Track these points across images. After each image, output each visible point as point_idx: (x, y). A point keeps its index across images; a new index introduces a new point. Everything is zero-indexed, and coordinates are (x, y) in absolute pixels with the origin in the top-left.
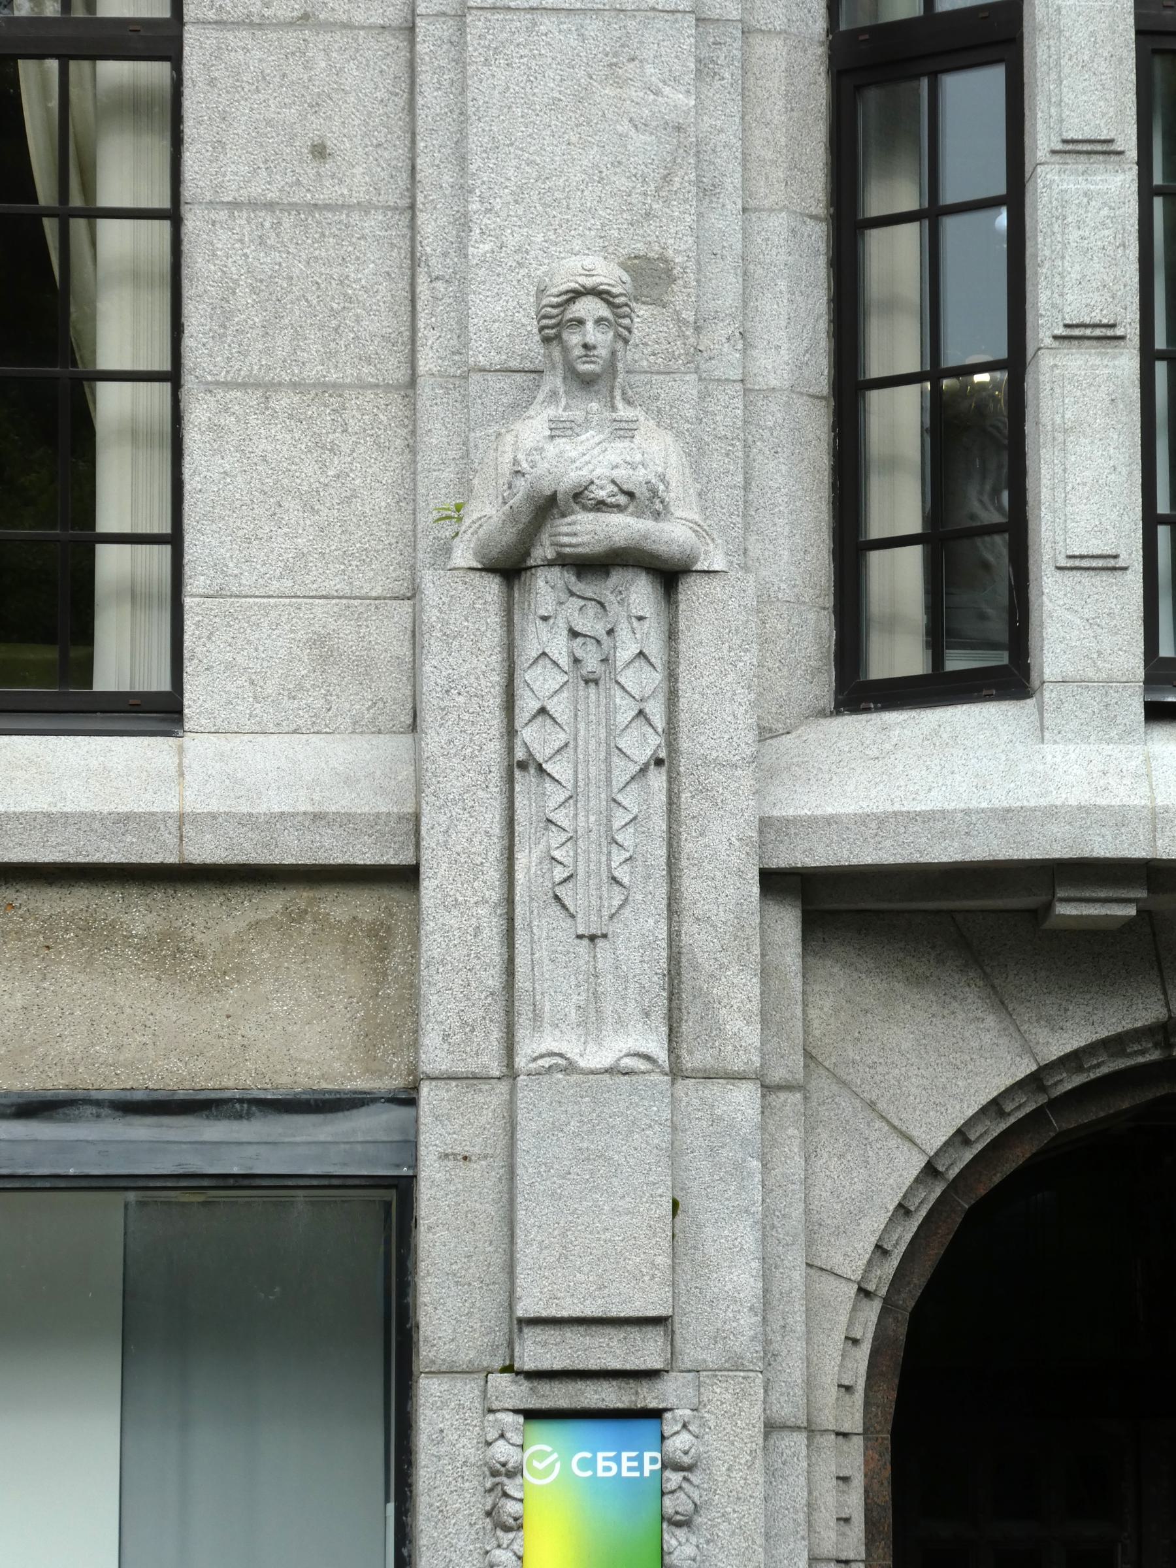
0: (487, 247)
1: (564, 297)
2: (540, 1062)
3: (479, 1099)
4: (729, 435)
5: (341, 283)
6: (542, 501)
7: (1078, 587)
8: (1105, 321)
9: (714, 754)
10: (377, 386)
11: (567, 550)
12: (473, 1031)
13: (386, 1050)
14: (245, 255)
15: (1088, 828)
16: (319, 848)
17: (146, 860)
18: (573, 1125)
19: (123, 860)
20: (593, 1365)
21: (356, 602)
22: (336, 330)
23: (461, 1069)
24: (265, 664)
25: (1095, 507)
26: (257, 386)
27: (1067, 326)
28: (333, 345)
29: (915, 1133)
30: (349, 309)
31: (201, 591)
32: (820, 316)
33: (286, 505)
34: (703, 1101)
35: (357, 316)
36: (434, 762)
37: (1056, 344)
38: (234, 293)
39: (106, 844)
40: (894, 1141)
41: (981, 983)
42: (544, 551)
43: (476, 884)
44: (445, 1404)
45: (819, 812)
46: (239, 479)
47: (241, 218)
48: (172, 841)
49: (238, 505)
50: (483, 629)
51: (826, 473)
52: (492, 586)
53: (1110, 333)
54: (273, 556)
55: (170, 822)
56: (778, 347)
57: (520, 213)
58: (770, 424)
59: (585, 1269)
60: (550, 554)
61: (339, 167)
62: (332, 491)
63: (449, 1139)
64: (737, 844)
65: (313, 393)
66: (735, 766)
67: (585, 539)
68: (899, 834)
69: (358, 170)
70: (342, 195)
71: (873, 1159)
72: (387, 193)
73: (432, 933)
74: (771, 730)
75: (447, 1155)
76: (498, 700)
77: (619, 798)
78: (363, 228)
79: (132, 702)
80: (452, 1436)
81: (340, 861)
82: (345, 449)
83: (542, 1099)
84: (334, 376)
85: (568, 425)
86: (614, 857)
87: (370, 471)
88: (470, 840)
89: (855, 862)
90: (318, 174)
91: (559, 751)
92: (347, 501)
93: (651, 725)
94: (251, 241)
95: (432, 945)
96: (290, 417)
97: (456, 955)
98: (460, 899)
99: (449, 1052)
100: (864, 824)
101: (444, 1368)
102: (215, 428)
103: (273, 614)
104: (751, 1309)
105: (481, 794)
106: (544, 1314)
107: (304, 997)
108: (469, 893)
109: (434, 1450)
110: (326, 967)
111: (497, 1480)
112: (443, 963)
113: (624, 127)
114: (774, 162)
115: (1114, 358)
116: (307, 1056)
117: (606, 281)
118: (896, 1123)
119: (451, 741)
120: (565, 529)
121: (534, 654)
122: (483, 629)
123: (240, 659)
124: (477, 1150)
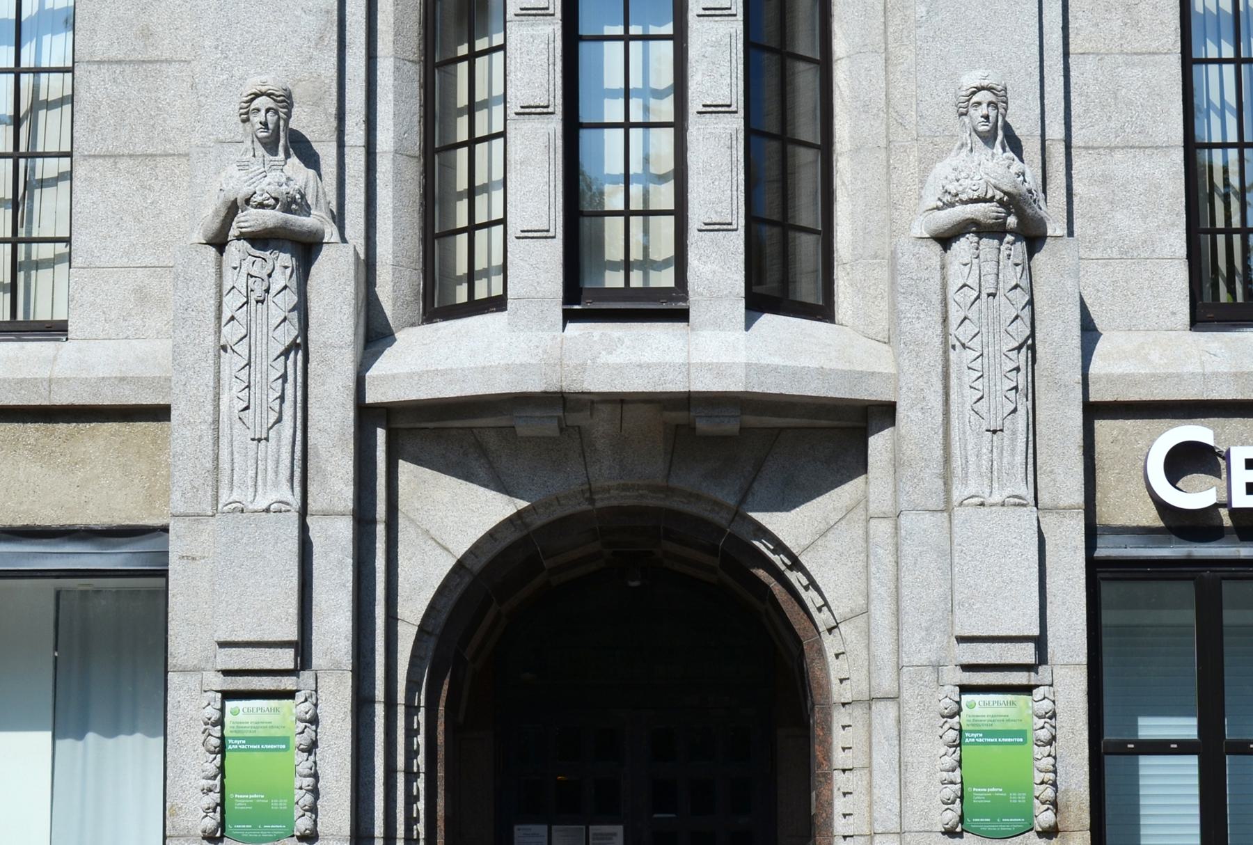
0: (225, 77)
1: (250, 97)
2: (229, 506)
3: (201, 527)
4: (357, 175)
5: (156, 101)
6: (230, 204)
7: (527, 248)
8: (542, 104)
9: (330, 341)
10: (174, 155)
11: (244, 230)
12: (197, 491)
13: (161, 504)
14: (106, 88)
15: (526, 376)
16: (123, 396)
17: (32, 403)
18: (245, 540)
19: (20, 404)
20: (256, 666)
21: (159, 269)
22: (153, 126)
23: (191, 511)
24: (111, 303)
25: (535, 204)
26: (111, 156)
27: (522, 107)
28: (151, 134)
29: (450, 547)
30: (160, 115)
31: (79, 265)
32: (415, 114)
33: (124, 218)
34: (321, 528)
35: (164, 118)
36: (179, 347)
37: (517, 117)
38: (100, 108)
39: (11, 395)
40: (439, 551)
41: (487, 466)
42: (234, 232)
43: (200, 413)
44: (181, 688)
45: (389, 373)
46: (101, 205)
47: (104, 68)
48: (45, 393)
49: (100, 219)
50: (206, 275)
51: (418, 197)
52: (212, 251)
53: (545, 110)
54: (118, 246)
55: (44, 383)
56: (388, 129)
57: (243, 58)
58: (383, 170)
59: (251, 616)
60: (237, 233)
61: (156, 41)
62: (150, 211)
63: (184, 549)
64: (342, 389)
65: (140, 159)
66: (341, 347)
67: (252, 223)
68: (429, 383)
69: (167, 41)
70: (157, 55)
71: (427, 561)
72: (181, 53)
73: (177, 439)
74: (382, 334)
75: (183, 557)
76: (214, 314)
77: (273, 364)
78: (168, 72)
79: (47, 325)
80: (183, 705)
81: (134, 403)
82: (157, 188)
83: (228, 526)
84: (151, 151)
85: (246, 163)
86: (270, 396)
87: (170, 200)
88: (197, 389)
89: (407, 399)
90: (145, 45)
91: (241, 339)
92: (157, 216)
93: (950, 520)
94: (109, 80)
95: (177, 446)
96: (128, 172)
97: (189, 451)
98: (192, 421)
99: (185, 502)
100: (412, 378)
101: (180, 669)
102: (89, 179)
103: (116, 276)
104: (346, 637)
105: (203, 364)
106: (229, 639)
107: (118, 476)
108: (197, 417)
109: (175, 712)
110: (129, 460)
111: (207, 727)
112: (182, 454)
113: (298, 13)
114: (387, 32)
115: (548, 123)
116: (118, 507)
117: (271, 88)
118: (441, 542)
119: (188, 336)
120: (242, 219)
121: (229, 288)
122: (206, 275)
123: (98, 300)
124: (199, 554)
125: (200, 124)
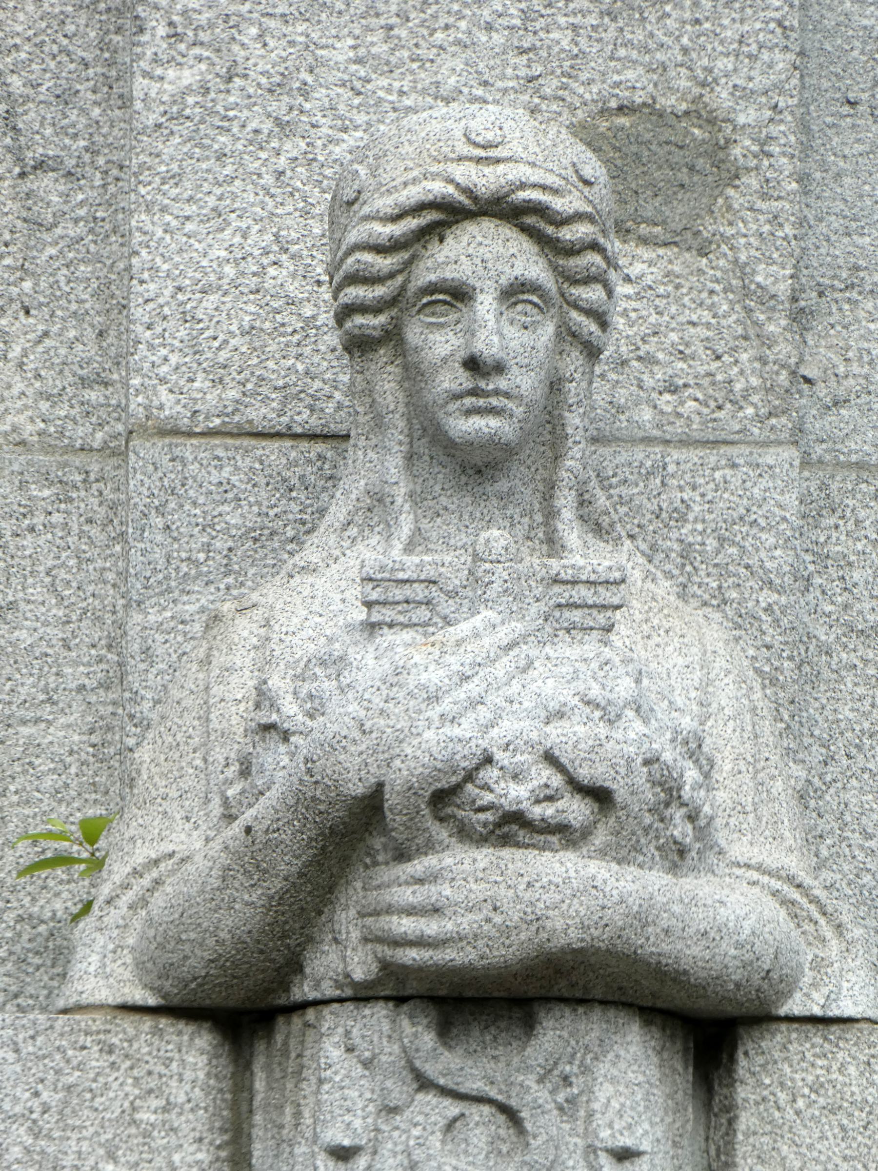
0: (188, 77)
1: (412, 223)
6: (338, 813)
11: (411, 955)
67: (466, 922)
85: (419, 592)
117: (535, 176)
120: (407, 895)
125: (36, 323)
